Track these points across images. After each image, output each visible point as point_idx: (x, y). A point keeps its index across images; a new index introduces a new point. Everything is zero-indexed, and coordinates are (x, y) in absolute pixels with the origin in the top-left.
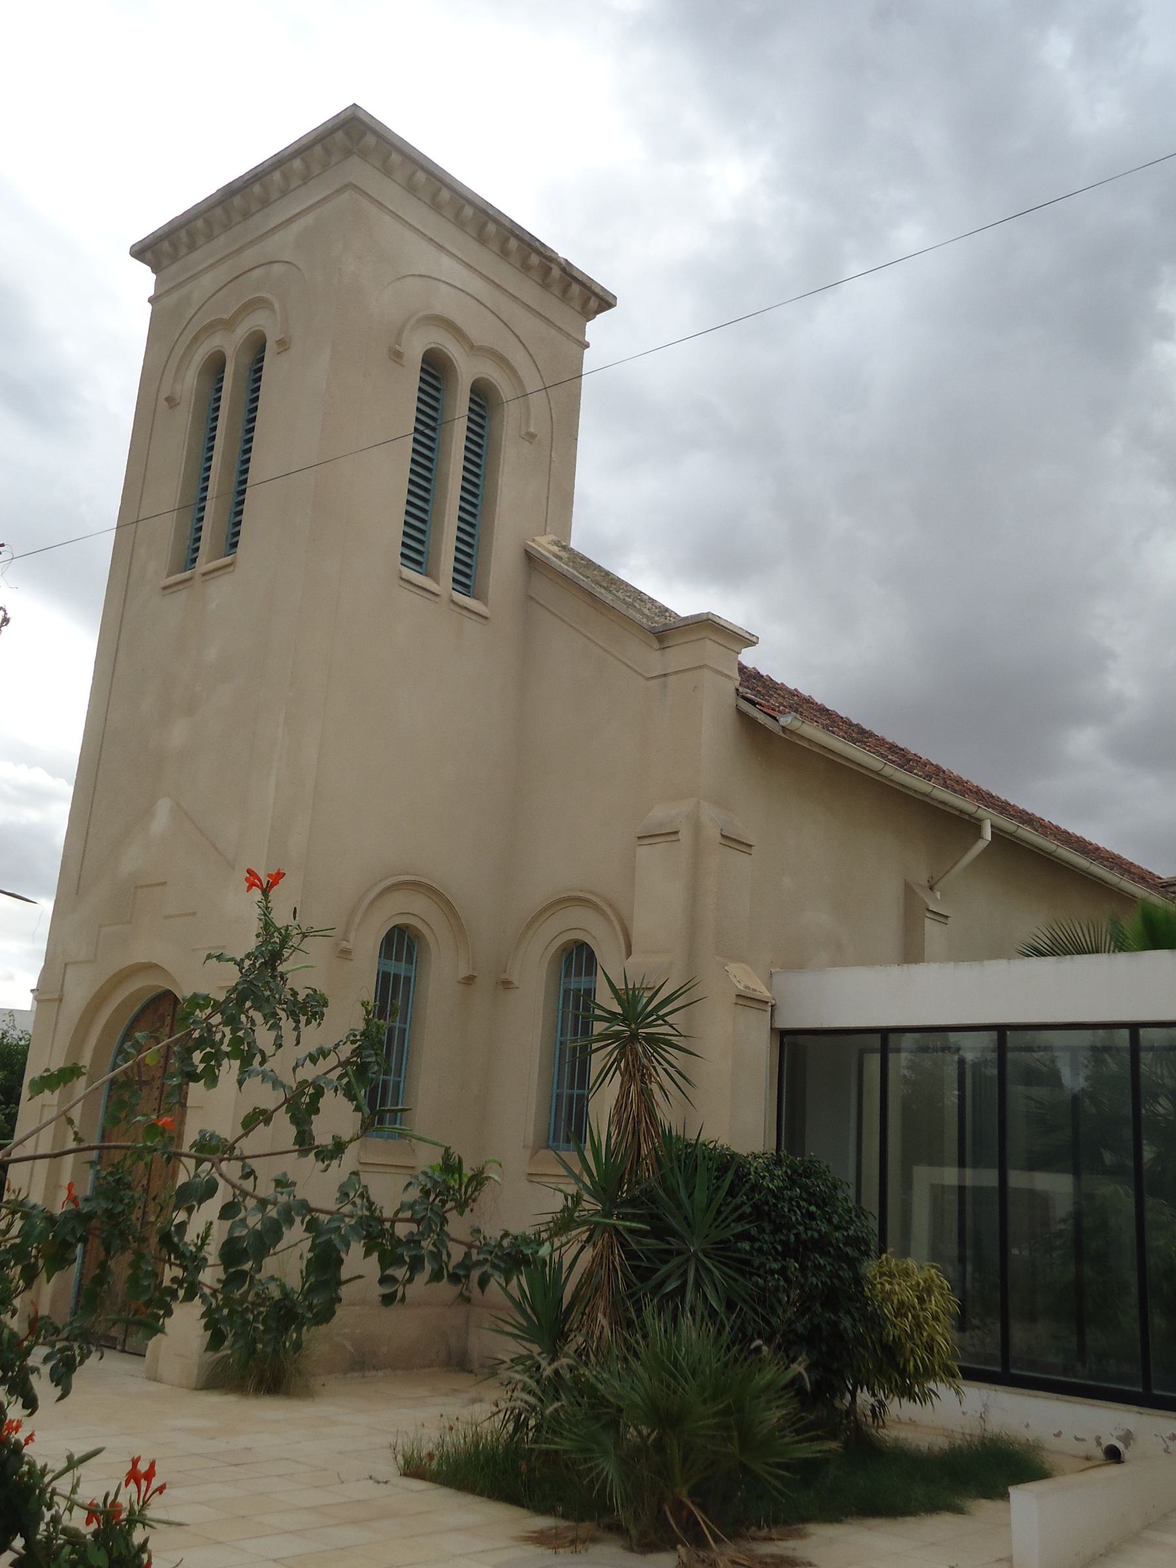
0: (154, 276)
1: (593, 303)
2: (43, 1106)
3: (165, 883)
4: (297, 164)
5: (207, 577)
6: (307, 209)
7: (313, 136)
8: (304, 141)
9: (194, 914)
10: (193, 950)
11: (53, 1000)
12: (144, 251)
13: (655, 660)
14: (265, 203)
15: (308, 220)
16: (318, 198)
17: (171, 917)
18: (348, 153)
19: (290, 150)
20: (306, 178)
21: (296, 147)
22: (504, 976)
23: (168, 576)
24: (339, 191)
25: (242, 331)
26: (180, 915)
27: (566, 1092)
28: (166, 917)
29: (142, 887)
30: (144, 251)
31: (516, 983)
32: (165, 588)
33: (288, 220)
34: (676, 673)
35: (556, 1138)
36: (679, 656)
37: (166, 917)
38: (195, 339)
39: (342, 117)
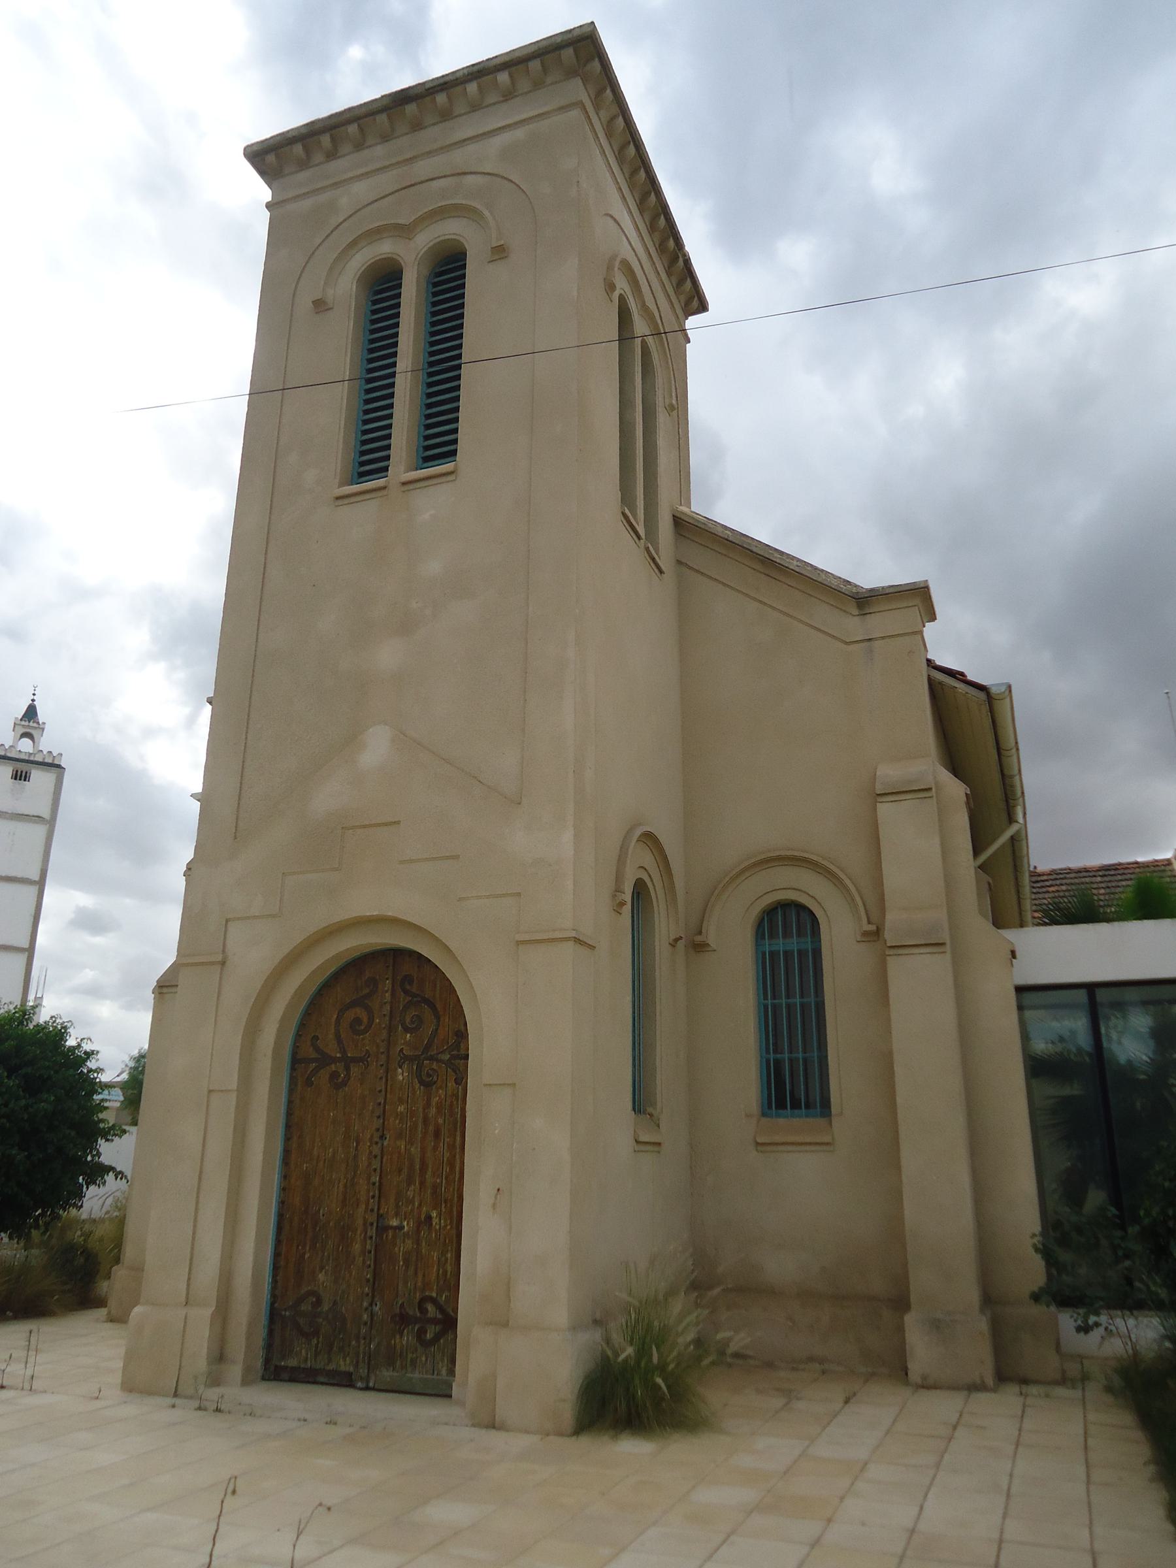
0: (264, 193)
1: (695, 303)
2: (210, 1091)
3: (398, 823)
4: (503, 77)
5: (340, 502)
6: (516, 123)
7: (533, 49)
8: (517, 54)
9: (456, 857)
10: (460, 899)
11: (212, 963)
12: (268, 157)
13: (853, 625)
14: (446, 115)
15: (520, 133)
16: (531, 114)
17: (411, 861)
18: (571, 73)
19: (498, 61)
20: (509, 95)
21: (507, 59)
22: (698, 939)
23: (340, 486)
24: (563, 109)
25: (425, 240)
26: (427, 859)
27: (772, 1056)
28: (402, 862)
29: (353, 828)
30: (268, 157)
31: (713, 945)
32: (337, 498)
33: (484, 134)
34: (883, 638)
35: (770, 1107)
36: (881, 622)
37: (402, 862)
38: (353, 244)
39: (575, 33)
